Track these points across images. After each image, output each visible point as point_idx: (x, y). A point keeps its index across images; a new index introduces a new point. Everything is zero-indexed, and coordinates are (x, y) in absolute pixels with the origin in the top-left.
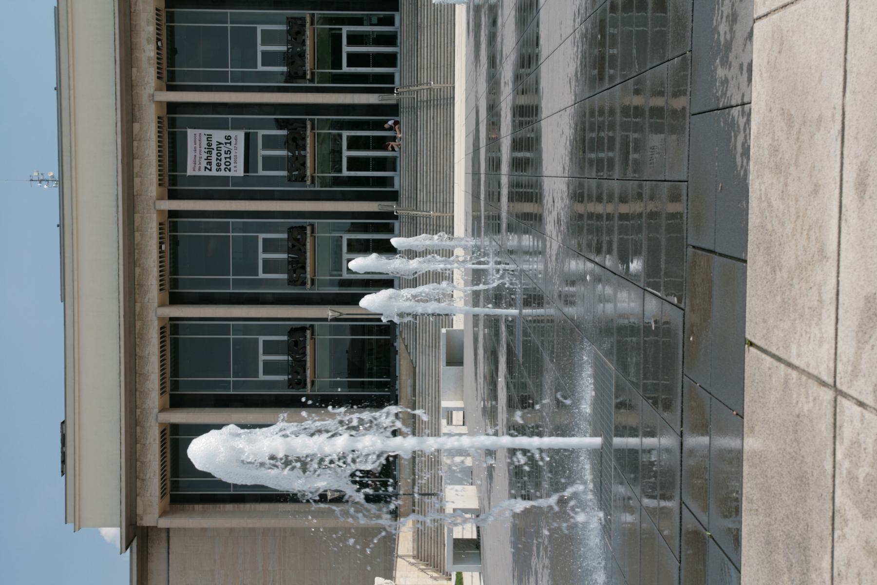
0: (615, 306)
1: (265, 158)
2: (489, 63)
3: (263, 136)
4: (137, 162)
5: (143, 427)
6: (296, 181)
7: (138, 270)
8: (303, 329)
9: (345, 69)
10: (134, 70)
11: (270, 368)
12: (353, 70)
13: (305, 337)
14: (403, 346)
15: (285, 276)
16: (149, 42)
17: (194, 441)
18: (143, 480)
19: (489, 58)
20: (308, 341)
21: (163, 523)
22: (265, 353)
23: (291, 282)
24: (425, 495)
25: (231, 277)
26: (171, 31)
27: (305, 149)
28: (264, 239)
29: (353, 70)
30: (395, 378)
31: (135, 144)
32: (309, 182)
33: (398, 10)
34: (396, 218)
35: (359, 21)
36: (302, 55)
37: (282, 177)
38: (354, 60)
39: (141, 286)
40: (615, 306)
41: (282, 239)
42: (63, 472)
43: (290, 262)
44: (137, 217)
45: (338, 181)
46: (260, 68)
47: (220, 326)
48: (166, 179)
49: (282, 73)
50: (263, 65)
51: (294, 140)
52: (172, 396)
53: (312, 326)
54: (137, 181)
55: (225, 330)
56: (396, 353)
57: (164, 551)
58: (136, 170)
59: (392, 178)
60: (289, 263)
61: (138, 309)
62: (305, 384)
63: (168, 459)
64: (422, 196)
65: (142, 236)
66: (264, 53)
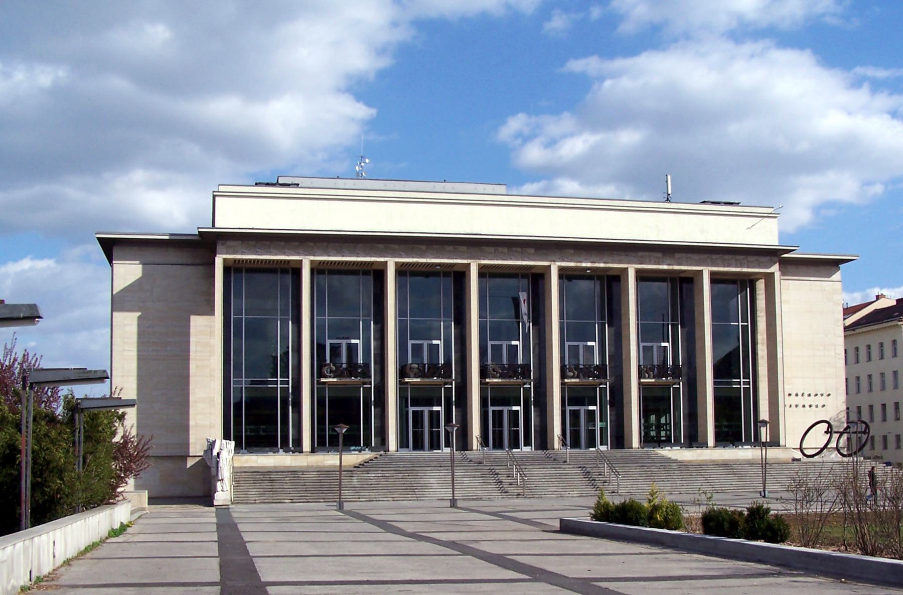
4: (505, 250)
10: (572, 251)
31: (519, 249)
44: (464, 248)
54: (492, 249)
58: (500, 249)
59: (408, 447)
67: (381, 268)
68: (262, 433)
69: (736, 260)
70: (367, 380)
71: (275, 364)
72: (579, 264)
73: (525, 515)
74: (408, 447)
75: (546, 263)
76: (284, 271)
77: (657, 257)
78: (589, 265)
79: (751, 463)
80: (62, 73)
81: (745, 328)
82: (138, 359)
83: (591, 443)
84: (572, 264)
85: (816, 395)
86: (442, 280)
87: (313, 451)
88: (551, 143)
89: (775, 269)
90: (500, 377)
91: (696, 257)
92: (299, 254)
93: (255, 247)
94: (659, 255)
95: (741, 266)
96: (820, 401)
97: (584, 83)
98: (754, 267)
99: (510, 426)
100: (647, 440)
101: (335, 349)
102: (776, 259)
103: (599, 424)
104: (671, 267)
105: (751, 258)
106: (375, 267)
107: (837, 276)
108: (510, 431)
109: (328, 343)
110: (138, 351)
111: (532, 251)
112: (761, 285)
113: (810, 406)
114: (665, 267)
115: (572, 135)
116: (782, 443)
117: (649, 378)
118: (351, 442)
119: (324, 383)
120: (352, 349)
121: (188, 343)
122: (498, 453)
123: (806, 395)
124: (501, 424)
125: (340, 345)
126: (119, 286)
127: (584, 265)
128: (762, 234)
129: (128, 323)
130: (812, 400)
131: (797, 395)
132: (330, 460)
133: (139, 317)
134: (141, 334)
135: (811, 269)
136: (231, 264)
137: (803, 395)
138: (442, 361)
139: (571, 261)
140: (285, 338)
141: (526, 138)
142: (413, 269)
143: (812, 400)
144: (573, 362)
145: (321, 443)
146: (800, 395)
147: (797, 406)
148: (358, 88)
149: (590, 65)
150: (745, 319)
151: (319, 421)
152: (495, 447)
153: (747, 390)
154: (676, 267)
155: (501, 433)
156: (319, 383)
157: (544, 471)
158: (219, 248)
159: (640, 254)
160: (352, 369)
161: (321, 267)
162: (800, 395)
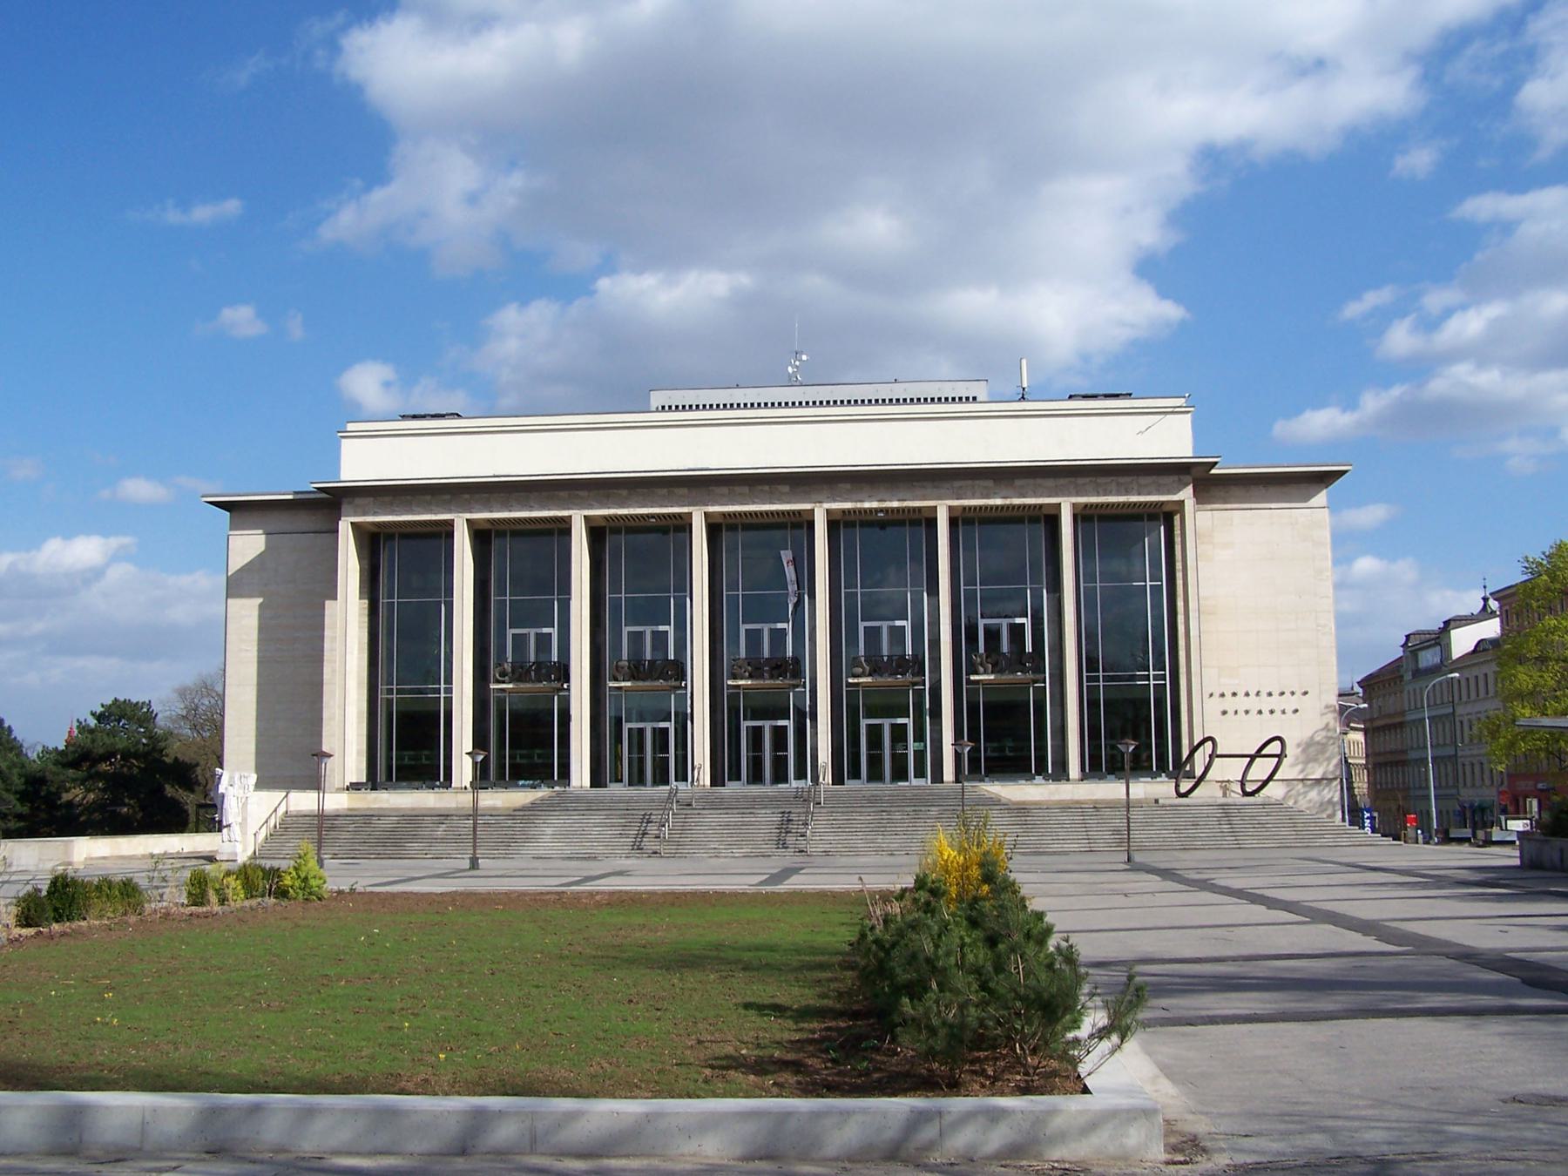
0: (1177, 786)
4: (746, 489)
7: (624, 492)
9: (864, 723)
10: (848, 486)
12: (863, 731)
17: (263, 548)
24: (320, 828)
26: (901, 523)
27: (772, 677)
29: (863, 731)
31: (766, 488)
35: (919, 737)
38: (875, 732)
39: (608, 497)
40: (1177, 786)
41: (880, 648)
44: (684, 491)
45: (734, 712)
46: (743, 628)
47: (684, 585)
48: (733, 521)
51: (778, 667)
52: (489, 531)
54: (725, 490)
57: (305, 529)
58: (738, 489)
59: (739, 779)
61: (581, 493)
63: (419, 529)
67: (1053, 512)
68: (1008, 753)
69: (1118, 484)
70: (1038, 676)
71: (1028, 658)
72: (859, 505)
73: (1237, 884)
74: (739, 779)
75: (808, 506)
76: (915, 523)
78: (875, 505)
79: (1111, 805)
80: (744, 280)
81: (1156, 590)
82: (259, 662)
83: (900, 774)
84: (848, 505)
85: (1282, 694)
86: (1026, 529)
88: (1431, 324)
89: (1186, 494)
90: (751, 677)
91: (1050, 482)
92: (450, 511)
93: (391, 504)
94: (990, 483)
95: (1127, 493)
96: (1289, 703)
97: (1472, 235)
98: (1149, 494)
99: (654, 752)
100: (971, 768)
101: (993, 635)
102: (1189, 478)
103: (912, 746)
104: (1008, 502)
105: (1144, 480)
106: (1045, 511)
107: (1321, 498)
108: (654, 759)
109: (981, 623)
110: (259, 651)
111: (786, 489)
112: (1177, 518)
113: (1272, 712)
114: (999, 502)
115: (1464, 307)
117: (985, 673)
118: (1139, 766)
119: (977, 682)
120: (1017, 631)
121: (322, 638)
122: (755, 790)
123: (1264, 694)
124: (641, 748)
125: (525, 637)
126: (235, 565)
127: (867, 505)
128: (1167, 437)
129: (245, 614)
130: (1276, 702)
131: (1247, 694)
132: (1110, 790)
133: (261, 605)
134: (262, 629)
135: (1272, 490)
136: (838, 517)
137: (1258, 694)
138: (789, 653)
139: (845, 501)
140: (1158, 618)
141: (1384, 317)
142: (983, 514)
143: (1276, 702)
144: (659, 656)
145: (1095, 768)
146: (1253, 694)
147: (1247, 712)
148: (1151, 269)
149: (1484, 206)
150: (1156, 577)
151: (1091, 733)
152: (655, 783)
153: (1160, 689)
154: (1017, 501)
155: (641, 761)
156: (969, 682)
157: (725, 818)
158: (345, 508)
159: (957, 484)
160: (1019, 659)
161: (1088, 512)
162: (1253, 694)
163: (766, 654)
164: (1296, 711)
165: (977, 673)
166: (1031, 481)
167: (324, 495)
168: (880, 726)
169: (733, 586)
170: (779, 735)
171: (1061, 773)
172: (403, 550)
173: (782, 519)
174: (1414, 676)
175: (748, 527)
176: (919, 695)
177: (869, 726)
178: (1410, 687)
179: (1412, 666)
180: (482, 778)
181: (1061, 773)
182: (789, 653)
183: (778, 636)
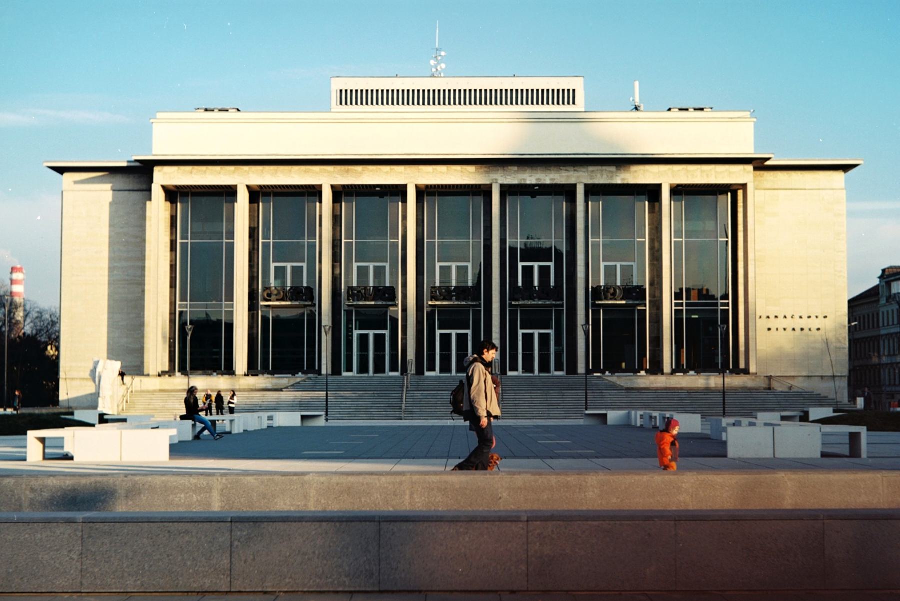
1: (450, 268)
2: (69, 519)
3: (467, 267)
5: (234, 172)
6: (432, 292)
8: (312, 299)
10: (516, 168)
11: (446, 271)
13: (306, 301)
14: (299, 380)
15: (355, 284)
16: (537, 180)
18: (191, 173)
19: (55, 518)
20: (303, 303)
21: (158, 193)
22: (293, 267)
23: (350, 288)
25: (189, 241)
28: (467, 267)
30: (272, 373)
32: (430, 303)
33: (567, 374)
34: (402, 374)
36: (531, 298)
37: (616, 280)
39: (348, 171)
41: (368, 281)
42: (227, 111)
43: (448, 289)
49: (450, 282)
50: (523, 267)
52: (258, 192)
53: (315, 305)
55: (678, 246)
56: (294, 375)
57: (122, 188)
60: (365, 288)
62: (267, 301)
63: (200, 190)
64: (418, 394)
65: (387, 173)
66: (450, 268)
69: (702, 172)
77: (612, 172)
86: (470, 200)
87: (673, 372)
112: (740, 193)
116: (753, 369)
159: (591, 169)
163: (454, 284)
164: (769, 329)
165: (518, 300)
166: (600, 168)
167: (138, 164)
168: (367, 336)
169: (432, 235)
170: (379, 339)
171: (657, 368)
172: (203, 204)
173: (302, 190)
174: (888, 301)
175: (277, 195)
176: (477, 314)
177: (441, 335)
178: (885, 310)
179: (886, 294)
180: (252, 370)
181: (657, 368)
182: (552, 284)
183: (379, 272)
